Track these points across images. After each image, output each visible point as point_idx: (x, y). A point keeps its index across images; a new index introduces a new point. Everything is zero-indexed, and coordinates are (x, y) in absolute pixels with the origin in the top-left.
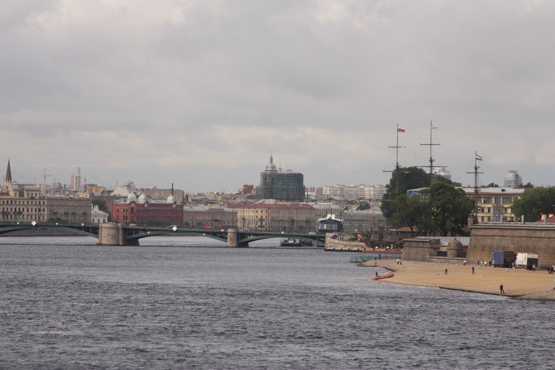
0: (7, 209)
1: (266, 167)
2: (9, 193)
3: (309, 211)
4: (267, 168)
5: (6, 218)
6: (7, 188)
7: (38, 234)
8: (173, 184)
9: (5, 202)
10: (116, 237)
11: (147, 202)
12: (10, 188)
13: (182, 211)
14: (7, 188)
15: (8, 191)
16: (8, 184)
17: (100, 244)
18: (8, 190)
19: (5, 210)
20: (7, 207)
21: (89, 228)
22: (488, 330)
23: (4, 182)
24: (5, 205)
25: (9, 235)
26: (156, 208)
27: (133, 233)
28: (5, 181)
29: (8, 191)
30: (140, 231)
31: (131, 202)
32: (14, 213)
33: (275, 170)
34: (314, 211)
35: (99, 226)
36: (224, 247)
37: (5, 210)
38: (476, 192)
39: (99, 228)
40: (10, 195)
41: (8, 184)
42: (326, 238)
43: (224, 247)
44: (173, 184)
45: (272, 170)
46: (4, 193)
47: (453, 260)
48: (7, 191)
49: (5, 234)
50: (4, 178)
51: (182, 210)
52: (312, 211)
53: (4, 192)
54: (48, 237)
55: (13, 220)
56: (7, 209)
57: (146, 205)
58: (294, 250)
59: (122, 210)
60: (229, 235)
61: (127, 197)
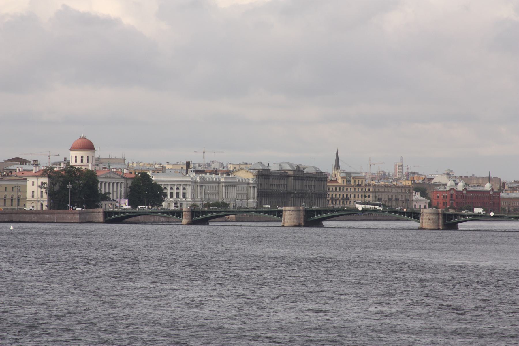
11: (465, 189)
13: (499, 198)
26: (474, 194)
31: (451, 189)
51: (499, 196)
57: (464, 192)
59: (442, 197)
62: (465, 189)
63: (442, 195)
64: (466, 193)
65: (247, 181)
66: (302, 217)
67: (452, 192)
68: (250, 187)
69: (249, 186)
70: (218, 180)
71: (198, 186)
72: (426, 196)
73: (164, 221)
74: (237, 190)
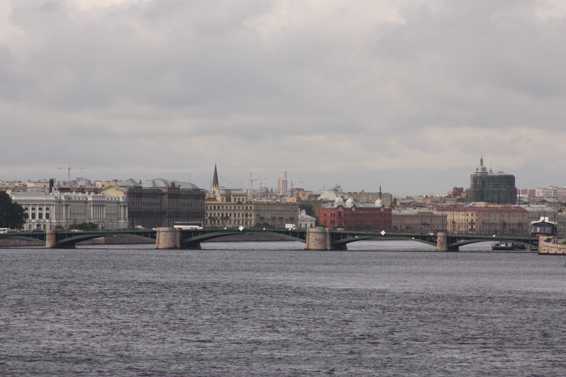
1: (476, 169)
3: (522, 213)
4: (477, 170)
8: (380, 187)
11: (354, 206)
13: (390, 215)
26: (364, 212)
33: (486, 172)
34: (527, 214)
36: (411, 251)
42: (539, 241)
43: (411, 251)
44: (380, 187)
45: (482, 172)
51: (391, 214)
52: (525, 213)
57: (353, 209)
59: (330, 214)
60: (439, 239)
62: (354, 206)
63: (329, 213)
64: (355, 211)
65: (117, 199)
66: (178, 238)
67: (340, 209)
68: (62, 205)
69: (119, 205)
70: (85, 199)
72: (312, 214)
73: (25, 245)
74: (106, 210)
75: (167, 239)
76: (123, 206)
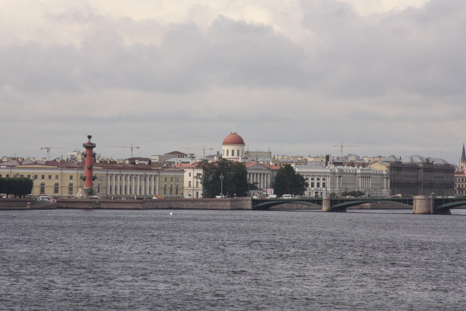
0: (463, 185)
2: (464, 172)
5: (461, 193)
6: (462, 168)
7: (390, 208)
9: (461, 180)
10: (428, 206)
12: (465, 168)
14: (462, 168)
15: (463, 171)
16: (463, 165)
17: (414, 213)
18: (463, 169)
19: (461, 186)
20: (463, 184)
21: (406, 200)
22: (423, 247)
23: (460, 163)
24: (460, 182)
25: (464, 207)
27: (443, 203)
28: (461, 162)
29: (463, 171)
30: (450, 201)
32: (458, 189)
35: (323, 198)
37: (461, 186)
38: (231, 167)
39: (322, 200)
40: (464, 174)
41: (463, 165)
46: (459, 172)
47: (362, 214)
48: (462, 171)
49: (461, 207)
50: (460, 159)
53: (460, 171)
54: (155, 210)
55: (457, 194)
56: (463, 185)
58: (298, 213)
61: (175, 162)
65: (381, 172)
66: (431, 205)
69: (383, 177)
71: (336, 177)
75: (422, 206)
76: (386, 178)
